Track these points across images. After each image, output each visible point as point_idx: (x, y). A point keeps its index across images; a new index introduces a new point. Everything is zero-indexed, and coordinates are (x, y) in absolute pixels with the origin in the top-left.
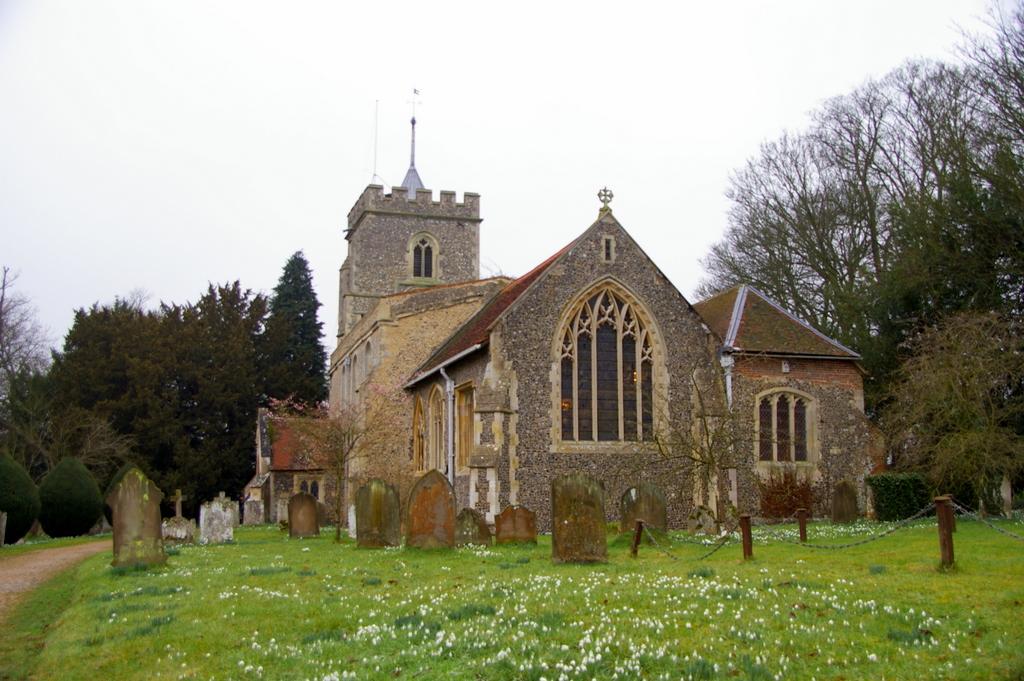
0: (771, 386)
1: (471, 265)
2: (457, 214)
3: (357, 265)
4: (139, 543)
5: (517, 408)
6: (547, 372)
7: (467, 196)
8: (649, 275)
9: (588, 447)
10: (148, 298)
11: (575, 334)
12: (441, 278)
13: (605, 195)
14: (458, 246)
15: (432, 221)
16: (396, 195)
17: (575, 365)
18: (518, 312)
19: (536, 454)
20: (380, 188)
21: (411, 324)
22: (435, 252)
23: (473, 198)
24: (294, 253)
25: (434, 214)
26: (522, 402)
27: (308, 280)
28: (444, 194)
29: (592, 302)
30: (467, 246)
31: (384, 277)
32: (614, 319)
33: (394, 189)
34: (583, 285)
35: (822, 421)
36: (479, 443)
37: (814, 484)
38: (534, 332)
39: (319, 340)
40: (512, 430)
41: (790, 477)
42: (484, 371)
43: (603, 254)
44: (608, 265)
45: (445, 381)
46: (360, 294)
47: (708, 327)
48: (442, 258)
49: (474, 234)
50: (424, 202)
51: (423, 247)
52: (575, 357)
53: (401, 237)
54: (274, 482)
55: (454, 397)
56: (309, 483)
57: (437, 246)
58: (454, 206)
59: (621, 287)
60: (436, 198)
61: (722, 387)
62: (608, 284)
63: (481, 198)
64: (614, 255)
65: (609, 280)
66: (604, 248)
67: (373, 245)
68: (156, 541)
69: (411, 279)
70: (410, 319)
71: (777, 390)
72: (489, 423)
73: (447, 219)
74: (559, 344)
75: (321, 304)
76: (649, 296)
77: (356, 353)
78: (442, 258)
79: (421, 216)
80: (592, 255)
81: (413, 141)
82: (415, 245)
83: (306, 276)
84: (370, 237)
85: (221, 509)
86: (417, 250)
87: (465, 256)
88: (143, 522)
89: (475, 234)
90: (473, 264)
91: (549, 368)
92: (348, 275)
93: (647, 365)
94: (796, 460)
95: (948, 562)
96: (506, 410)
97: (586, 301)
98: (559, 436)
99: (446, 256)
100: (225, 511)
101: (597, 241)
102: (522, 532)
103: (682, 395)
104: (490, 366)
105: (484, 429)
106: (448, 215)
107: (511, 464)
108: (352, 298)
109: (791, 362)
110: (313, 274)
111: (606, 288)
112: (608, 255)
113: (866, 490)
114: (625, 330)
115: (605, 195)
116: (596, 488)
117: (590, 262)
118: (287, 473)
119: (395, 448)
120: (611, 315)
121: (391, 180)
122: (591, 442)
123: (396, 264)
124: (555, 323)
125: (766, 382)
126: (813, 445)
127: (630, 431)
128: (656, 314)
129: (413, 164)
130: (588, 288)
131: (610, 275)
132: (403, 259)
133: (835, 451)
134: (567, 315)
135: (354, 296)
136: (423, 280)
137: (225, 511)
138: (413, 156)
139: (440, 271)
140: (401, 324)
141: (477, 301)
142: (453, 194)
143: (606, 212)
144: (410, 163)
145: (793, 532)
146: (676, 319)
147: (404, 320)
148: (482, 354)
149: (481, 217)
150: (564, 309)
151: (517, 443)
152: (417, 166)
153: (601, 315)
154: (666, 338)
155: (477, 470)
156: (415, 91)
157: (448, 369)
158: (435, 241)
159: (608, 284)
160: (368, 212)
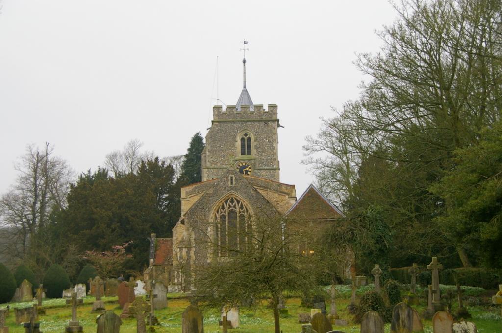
1: (272, 146)
2: (264, 118)
3: (209, 151)
5: (194, 245)
8: (249, 190)
10: (140, 146)
15: (250, 123)
19: (202, 263)
22: (252, 141)
23: (273, 107)
24: (195, 134)
25: (250, 119)
29: (226, 202)
31: (224, 157)
34: (221, 196)
43: (230, 183)
46: (211, 167)
48: (256, 143)
51: (246, 138)
58: (262, 113)
62: (232, 194)
64: (234, 183)
67: (217, 140)
69: (240, 156)
70: (194, 197)
73: (257, 121)
76: (249, 198)
78: (256, 143)
79: (243, 121)
80: (225, 183)
82: (241, 137)
86: (243, 140)
99: (259, 142)
101: (227, 177)
106: (259, 119)
108: (207, 169)
111: (231, 196)
112: (232, 183)
114: (240, 212)
117: (224, 186)
120: (235, 207)
121: (230, 99)
129: (245, 87)
130: (223, 196)
132: (234, 145)
134: (214, 208)
135: (208, 168)
136: (246, 157)
138: (245, 82)
142: (261, 106)
146: (261, 207)
151: (194, 259)
153: (230, 207)
156: (245, 43)
158: (251, 134)
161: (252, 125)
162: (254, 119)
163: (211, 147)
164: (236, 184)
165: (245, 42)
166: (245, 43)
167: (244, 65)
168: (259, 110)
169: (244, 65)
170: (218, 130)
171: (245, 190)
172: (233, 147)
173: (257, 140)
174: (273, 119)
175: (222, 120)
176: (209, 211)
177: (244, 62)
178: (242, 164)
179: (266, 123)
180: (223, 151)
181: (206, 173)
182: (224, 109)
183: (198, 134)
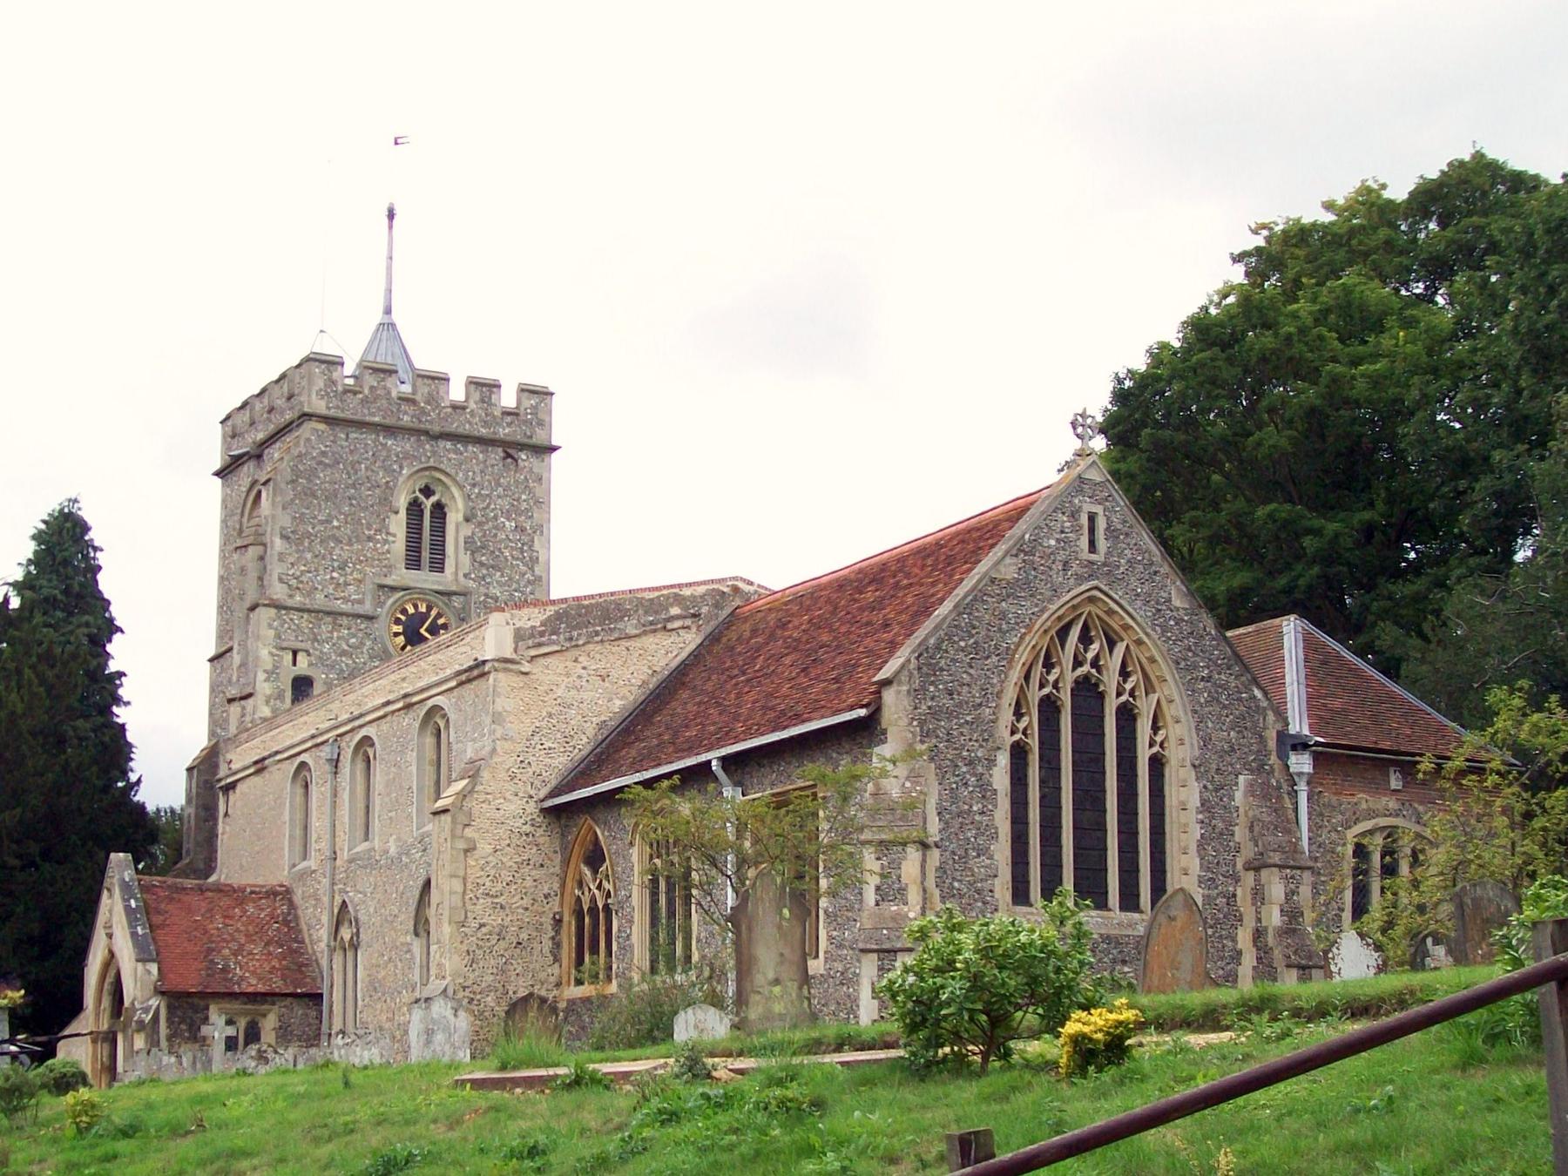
0: (1371, 814)
2: (503, 432)
3: (284, 537)
4: (777, 990)
6: (989, 768)
11: (1035, 695)
12: (465, 576)
14: (505, 503)
15: (449, 445)
16: (370, 380)
18: (938, 647)
20: (334, 363)
21: (553, 673)
22: (454, 517)
25: (453, 427)
26: (947, 825)
28: (474, 384)
29: (1063, 633)
30: (524, 506)
36: (872, 903)
39: (115, 709)
43: (1084, 542)
44: (1092, 563)
46: (290, 603)
47: (1265, 693)
48: (467, 530)
50: (432, 399)
51: (428, 504)
52: (1034, 743)
53: (382, 477)
54: (168, 1019)
57: (460, 504)
58: (497, 413)
60: (457, 392)
61: (1291, 815)
62: (1092, 600)
63: (556, 402)
64: (1102, 544)
68: (800, 988)
70: (549, 660)
71: (1383, 821)
72: (896, 865)
74: (1007, 716)
78: (467, 530)
79: (426, 433)
84: (312, 474)
85: (449, 1013)
86: (415, 508)
87: (520, 529)
88: (782, 955)
90: (537, 546)
91: (991, 762)
92: (262, 558)
93: (1157, 763)
97: (1053, 632)
98: (1008, 897)
99: (480, 524)
101: (1074, 515)
103: (1221, 825)
108: (273, 611)
110: (102, 559)
112: (1092, 547)
116: (1509, 905)
117: (1062, 556)
118: (196, 1001)
119: (524, 936)
120: (1095, 664)
121: (351, 349)
123: (370, 538)
124: (1004, 673)
125: (1364, 806)
129: (388, 311)
131: (1095, 583)
132: (383, 528)
135: (279, 606)
136: (425, 579)
137: (455, 1015)
138: (389, 291)
139: (465, 559)
141: (688, 627)
142: (495, 386)
144: (381, 309)
147: (542, 661)
149: (554, 443)
150: (1018, 645)
152: (396, 317)
153: (1078, 663)
155: (875, 956)
157: (727, 762)
159: (1092, 600)
160: (306, 416)
161: (457, 452)
162: (466, 429)
164: (1109, 553)
165: (396, 140)
166: (396, 143)
167: (391, 227)
168: (486, 401)
170: (324, 454)
171: (1146, 588)
172: (379, 531)
173: (475, 516)
174: (534, 441)
175: (341, 415)
177: (391, 215)
178: (416, 606)
179: (508, 456)
180: (338, 541)
181: (270, 626)
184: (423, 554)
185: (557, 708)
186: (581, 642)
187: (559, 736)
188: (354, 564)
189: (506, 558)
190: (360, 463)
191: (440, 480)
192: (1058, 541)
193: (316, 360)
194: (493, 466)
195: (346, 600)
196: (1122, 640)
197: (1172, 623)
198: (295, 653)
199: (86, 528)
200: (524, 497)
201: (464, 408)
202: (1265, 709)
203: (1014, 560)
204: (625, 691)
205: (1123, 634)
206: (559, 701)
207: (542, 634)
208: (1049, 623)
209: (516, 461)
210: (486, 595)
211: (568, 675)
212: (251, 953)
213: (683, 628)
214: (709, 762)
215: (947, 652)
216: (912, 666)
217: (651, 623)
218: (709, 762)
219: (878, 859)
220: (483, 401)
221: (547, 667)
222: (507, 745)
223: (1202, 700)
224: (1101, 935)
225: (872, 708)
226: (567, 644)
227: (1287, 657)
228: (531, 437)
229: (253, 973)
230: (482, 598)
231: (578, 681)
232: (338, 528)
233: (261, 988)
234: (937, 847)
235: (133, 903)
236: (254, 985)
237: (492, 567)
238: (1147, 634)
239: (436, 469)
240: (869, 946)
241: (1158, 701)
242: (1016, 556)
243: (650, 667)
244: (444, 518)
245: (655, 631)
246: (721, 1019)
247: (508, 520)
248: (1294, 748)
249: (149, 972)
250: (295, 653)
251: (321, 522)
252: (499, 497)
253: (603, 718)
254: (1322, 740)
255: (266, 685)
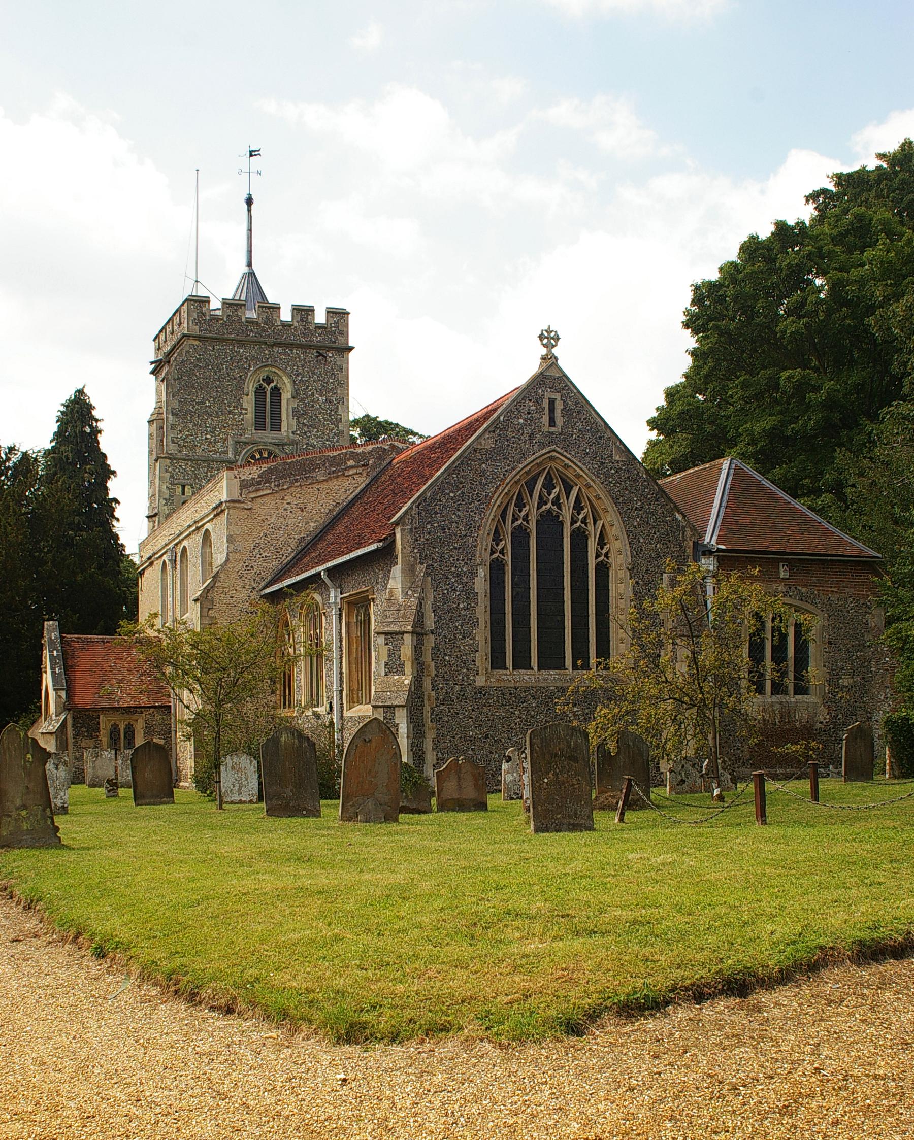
4: (24, 813)
5: (433, 627)
7: (331, 312)
9: (526, 677)
11: (509, 527)
13: (549, 338)
15: (280, 350)
17: (509, 569)
18: (433, 499)
22: (286, 396)
23: (339, 316)
27: (96, 432)
29: (531, 484)
30: (331, 386)
32: (560, 508)
33: (226, 303)
35: (830, 643)
37: (819, 726)
38: (454, 525)
40: (427, 657)
41: (787, 713)
42: (387, 577)
43: (545, 419)
44: (553, 433)
45: (327, 589)
46: (179, 456)
47: (684, 516)
49: (341, 369)
50: (269, 321)
52: (508, 559)
54: (73, 725)
55: (340, 609)
56: (122, 727)
58: (312, 328)
59: (570, 464)
60: (286, 315)
62: (552, 459)
64: (559, 421)
65: (554, 454)
66: (547, 411)
68: (44, 810)
69: (250, 433)
70: (266, 499)
72: (397, 648)
74: (484, 539)
75: (114, 472)
76: (607, 476)
77: (185, 543)
81: (250, 230)
83: (91, 426)
84: (191, 373)
86: (260, 392)
89: (343, 370)
91: (474, 574)
93: (603, 570)
94: (795, 694)
95: (815, 795)
96: (419, 630)
99: (302, 400)
100: (57, 769)
101: (538, 402)
102: (470, 792)
104: (397, 571)
105: (389, 656)
107: (426, 701)
109: (791, 564)
112: (552, 422)
113: (786, 631)
114: (573, 522)
115: (549, 338)
117: (527, 430)
120: (556, 502)
122: (529, 672)
126: (815, 671)
127: (580, 653)
128: (615, 501)
129: (250, 265)
132: (239, 405)
133: (845, 681)
136: (268, 436)
137: (57, 769)
138: (250, 252)
139: (294, 422)
140: (256, 506)
143: (550, 361)
145: (805, 785)
148: (386, 555)
149: (350, 344)
153: (542, 502)
154: (628, 532)
163: (180, 402)
164: (565, 425)
165: (251, 152)
166: (251, 155)
167: (249, 210)
169: (249, 210)
176: (481, 512)
177: (249, 201)
179: (321, 355)
182: (215, 304)
183: (81, 392)
184: (267, 420)
185: (271, 530)
186: (285, 487)
187: (272, 548)
188: (221, 429)
189: (319, 420)
190: (222, 365)
191: (275, 372)
192: (525, 420)
193: (191, 300)
194: (309, 362)
195: (216, 452)
196: (577, 485)
197: (613, 471)
198: (183, 487)
199: (90, 407)
200: (331, 381)
201: (290, 326)
202: (684, 527)
203: (492, 435)
204: (316, 517)
205: (576, 481)
206: (272, 525)
207: (259, 483)
208: (518, 477)
209: (326, 357)
210: (307, 444)
211: (277, 509)
212: (129, 681)
213: (356, 474)
214: (319, 573)
215: (440, 501)
216: (413, 512)
217: (334, 472)
218: (319, 573)
219: (387, 644)
220: (302, 320)
221: (263, 505)
222: (238, 556)
223: (635, 523)
224: (557, 687)
225: (388, 542)
226: (276, 489)
227: (719, 485)
228: (335, 342)
229: (128, 694)
230: (305, 446)
231: (285, 512)
232: (209, 407)
233: (132, 704)
234: (432, 633)
235: (55, 653)
236: (129, 702)
237: (311, 426)
238: (593, 480)
239: (272, 366)
240: (377, 704)
241: (603, 525)
242: (494, 432)
243: (334, 501)
244: (280, 397)
245: (337, 477)
246: (251, 762)
247: (321, 396)
248: (704, 554)
249: (60, 697)
250: (183, 487)
251: (198, 404)
252: (314, 381)
253: (302, 535)
254: (723, 547)
255: (165, 507)
